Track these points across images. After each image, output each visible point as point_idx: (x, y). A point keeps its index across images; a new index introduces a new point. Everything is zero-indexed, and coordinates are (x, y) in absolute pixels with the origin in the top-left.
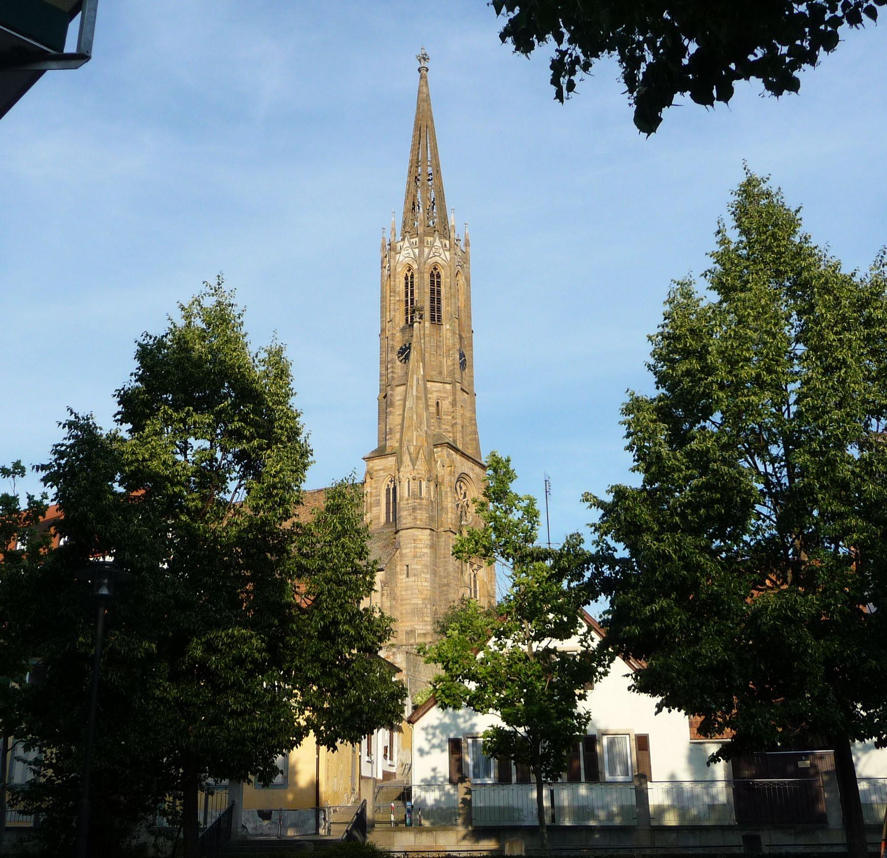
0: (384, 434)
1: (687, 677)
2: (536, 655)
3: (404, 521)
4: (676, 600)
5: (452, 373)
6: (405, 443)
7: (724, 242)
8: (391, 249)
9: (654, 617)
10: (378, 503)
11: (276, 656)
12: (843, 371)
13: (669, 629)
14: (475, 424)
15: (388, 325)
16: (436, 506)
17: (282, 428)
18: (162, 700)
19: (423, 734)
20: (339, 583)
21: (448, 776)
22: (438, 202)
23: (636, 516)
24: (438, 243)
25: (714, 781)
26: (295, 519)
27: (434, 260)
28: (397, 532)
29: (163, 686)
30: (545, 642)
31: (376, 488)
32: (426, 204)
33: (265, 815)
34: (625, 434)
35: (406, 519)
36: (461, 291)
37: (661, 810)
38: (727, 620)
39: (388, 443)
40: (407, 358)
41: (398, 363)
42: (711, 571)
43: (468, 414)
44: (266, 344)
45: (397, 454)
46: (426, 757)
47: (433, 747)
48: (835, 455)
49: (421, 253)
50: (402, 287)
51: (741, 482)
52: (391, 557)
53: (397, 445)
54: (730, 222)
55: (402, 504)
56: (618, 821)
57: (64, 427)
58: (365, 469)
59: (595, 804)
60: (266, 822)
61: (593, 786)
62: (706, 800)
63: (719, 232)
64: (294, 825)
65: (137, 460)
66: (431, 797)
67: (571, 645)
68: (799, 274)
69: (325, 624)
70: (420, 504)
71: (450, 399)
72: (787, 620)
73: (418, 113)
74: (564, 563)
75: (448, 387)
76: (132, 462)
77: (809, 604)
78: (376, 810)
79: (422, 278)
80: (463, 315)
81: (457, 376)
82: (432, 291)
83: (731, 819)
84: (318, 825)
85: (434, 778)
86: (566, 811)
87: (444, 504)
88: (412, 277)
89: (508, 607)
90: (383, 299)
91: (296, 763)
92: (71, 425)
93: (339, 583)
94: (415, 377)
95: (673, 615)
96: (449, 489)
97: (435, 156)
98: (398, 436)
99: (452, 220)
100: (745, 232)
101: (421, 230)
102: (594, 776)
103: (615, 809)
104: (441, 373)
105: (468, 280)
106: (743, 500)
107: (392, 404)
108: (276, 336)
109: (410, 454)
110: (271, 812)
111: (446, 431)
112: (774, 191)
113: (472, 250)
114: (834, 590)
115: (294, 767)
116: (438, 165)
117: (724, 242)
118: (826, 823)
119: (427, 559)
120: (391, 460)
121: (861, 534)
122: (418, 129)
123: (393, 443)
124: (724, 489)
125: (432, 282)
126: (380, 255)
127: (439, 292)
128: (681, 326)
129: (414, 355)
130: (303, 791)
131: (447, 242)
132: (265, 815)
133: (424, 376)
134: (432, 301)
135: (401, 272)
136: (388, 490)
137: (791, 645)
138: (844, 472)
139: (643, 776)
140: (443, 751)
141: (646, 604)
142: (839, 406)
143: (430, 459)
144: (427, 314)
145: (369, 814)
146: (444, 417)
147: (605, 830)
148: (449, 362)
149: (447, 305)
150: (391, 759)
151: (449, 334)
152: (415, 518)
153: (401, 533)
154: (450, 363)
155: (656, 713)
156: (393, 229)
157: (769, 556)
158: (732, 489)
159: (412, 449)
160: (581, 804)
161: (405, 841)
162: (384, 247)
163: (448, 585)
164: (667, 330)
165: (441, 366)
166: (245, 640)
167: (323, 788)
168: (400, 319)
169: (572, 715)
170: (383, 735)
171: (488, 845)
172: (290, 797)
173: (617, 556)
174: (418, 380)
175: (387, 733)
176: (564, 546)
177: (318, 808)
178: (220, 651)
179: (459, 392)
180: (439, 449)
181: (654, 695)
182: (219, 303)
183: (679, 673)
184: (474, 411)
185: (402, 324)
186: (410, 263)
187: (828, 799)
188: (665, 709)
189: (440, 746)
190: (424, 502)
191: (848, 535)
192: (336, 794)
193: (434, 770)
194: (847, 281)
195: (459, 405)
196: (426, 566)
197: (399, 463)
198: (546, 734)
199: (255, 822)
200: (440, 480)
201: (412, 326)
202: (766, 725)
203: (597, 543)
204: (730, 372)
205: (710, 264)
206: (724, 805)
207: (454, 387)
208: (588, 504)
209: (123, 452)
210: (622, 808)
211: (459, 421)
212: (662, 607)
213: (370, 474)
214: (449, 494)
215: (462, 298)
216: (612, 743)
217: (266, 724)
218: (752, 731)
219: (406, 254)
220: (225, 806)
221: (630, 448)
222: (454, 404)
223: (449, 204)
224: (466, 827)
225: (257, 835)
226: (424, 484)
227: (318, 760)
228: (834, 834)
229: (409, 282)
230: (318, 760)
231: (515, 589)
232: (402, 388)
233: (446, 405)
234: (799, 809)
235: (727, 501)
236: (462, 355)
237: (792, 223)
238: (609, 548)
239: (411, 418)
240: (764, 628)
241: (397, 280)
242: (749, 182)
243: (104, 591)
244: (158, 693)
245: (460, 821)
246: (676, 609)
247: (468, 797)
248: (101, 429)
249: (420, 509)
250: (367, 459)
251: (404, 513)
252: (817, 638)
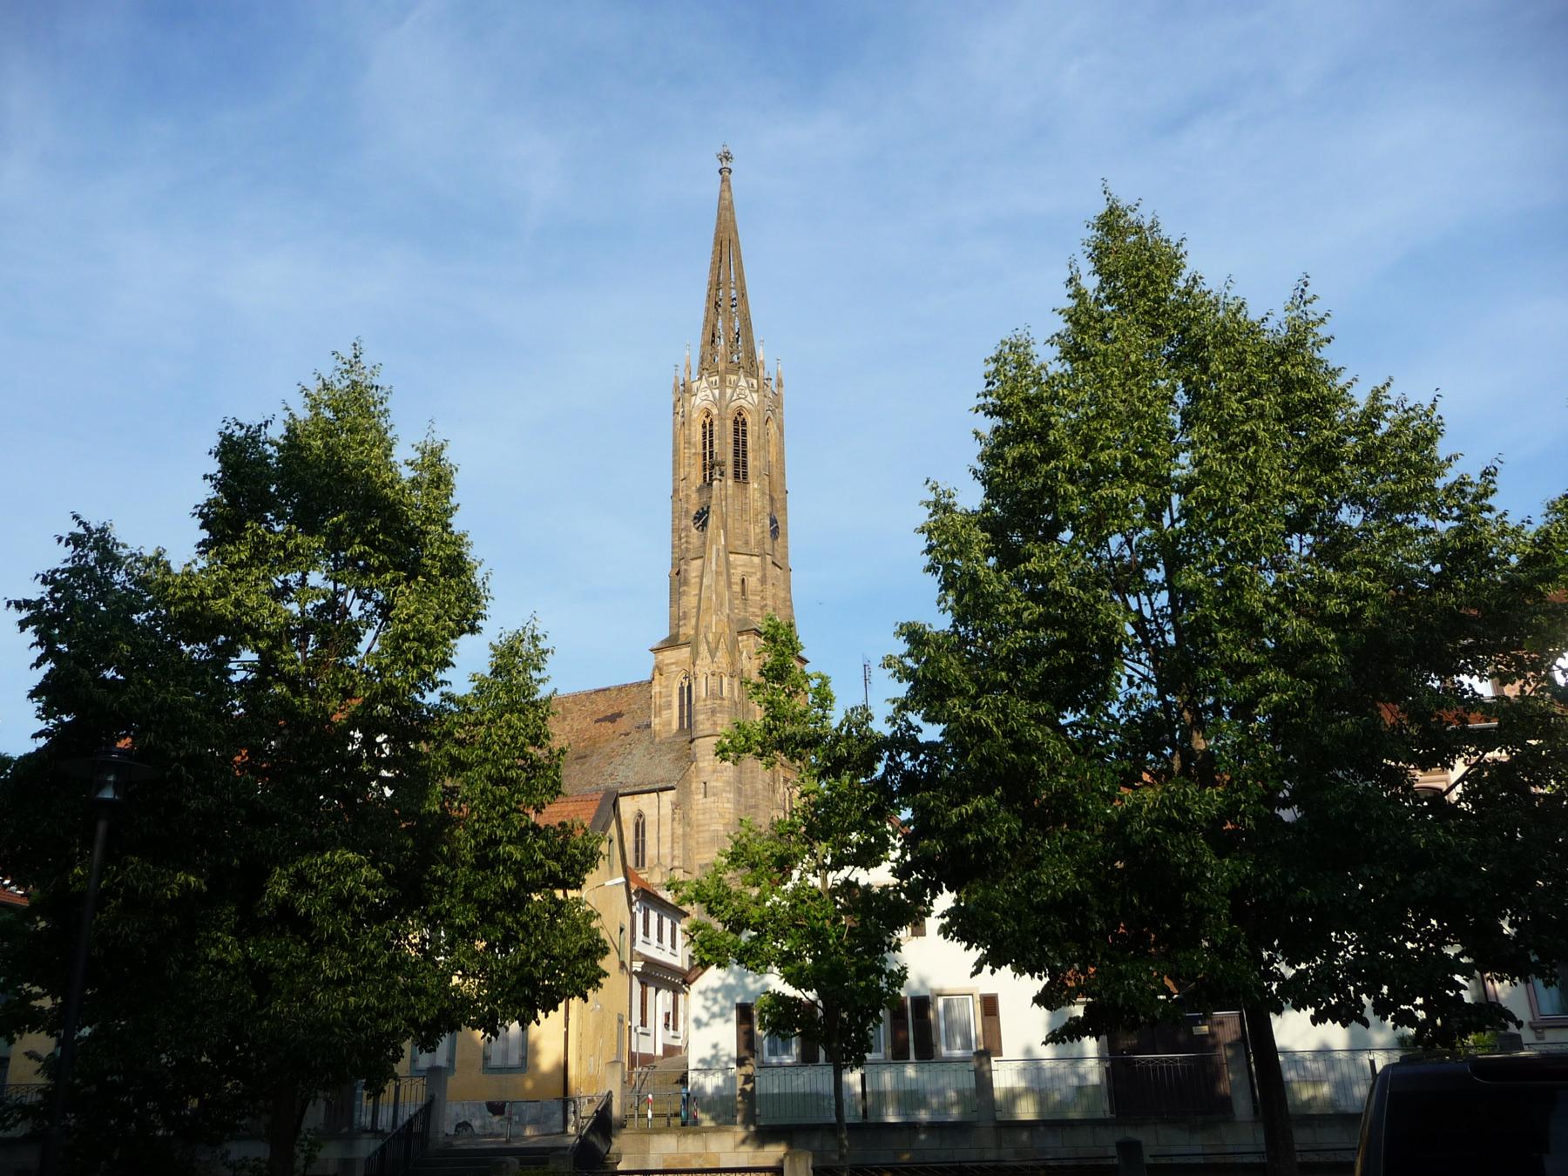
0: (677, 620)
1: (1018, 918)
2: (833, 892)
4: (1000, 800)
5: (761, 543)
6: (702, 630)
7: (1079, 295)
8: (685, 390)
9: (962, 827)
10: (669, 706)
11: (411, 892)
12: (1252, 450)
13: (989, 844)
15: (682, 484)
17: (434, 557)
18: (221, 964)
19: (701, 998)
20: (503, 781)
21: (734, 1054)
22: (743, 336)
23: (940, 670)
24: (743, 383)
25: (1082, 1058)
26: (445, 689)
27: (738, 403)
28: (692, 741)
29: (223, 943)
30: (846, 872)
32: (728, 338)
33: (496, 1108)
34: (925, 547)
36: (772, 442)
37: (1013, 1096)
38: (1082, 829)
39: (682, 631)
40: (705, 524)
42: (1055, 753)
43: (782, 594)
44: (419, 439)
45: (692, 643)
46: (703, 1030)
47: (713, 1016)
48: (1243, 572)
49: (722, 394)
50: (699, 437)
51: (1098, 612)
52: (685, 773)
53: (692, 632)
54: (1086, 266)
55: (698, 706)
56: (955, 1113)
57: (67, 544)
58: (653, 663)
59: (928, 1087)
60: (497, 1118)
61: (926, 1067)
62: (1074, 1081)
63: (1070, 281)
64: (535, 1122)
65: (191, 598)
66: (711, 1083)
67: (880, 876)
68: (1184, 331)
69: (478, 843)
71: (759, 575)
72: (1171, 826)
73: (719, 224)
74: (842, 750)
75: (756, 560)
76: (183, 600)
77: (1207, 800)
78: (623, 1106)
79: (723, 425)
80: (775, 472)
81: (768, 547)
82: (736, 442)
83: (1104, 1109)
84: (566, 1122)
85: (715, 1057)
86: (889, 1098)
88: (711, 424)
89: (790, 824)
90: (676, 452)
91: (538, 1038)
92: (75, 540)
93: (503, 781)
95: (998, 821)
97: (740, 276)
98: (693, 621)
99: (760, 354)
100: (1108, 276)
101: (721, 367)
102: (926, 1052)
103: (952, 1095)
104: (747, 543)
105: (780, 429)
106: (1102, 639)
107: (686, 582)
108: (434, 427)
110: (504, 1104)
111: (754, 614)
112: (1147, 224)
113: (784, 392)
114: (1245, 780)
115: (534, 1044)
116: (743, 288)
117: (1079, 295)
118: (1231, 1110)
120: (685, 652)
121: (1284, 692)
122: (719, 242)
123: (687, 630)
124: (1073, 625)
125: (736, 431)
126: (672, 399)
127: (745, 444)
128: (1011, 394)
129: (713, 520)
130: (546, 1077)
132: (496, 1108)
133: (726, 546)
134: (736, 453)
135: (698, 419)
136: (681, 689)
137: (1178, 866)
138: (1254, 600)
139: (990, 1049)
140: (727, 1021)
141: (953, 804)
142: (1247, 499)
143: (734, 649)
144: (730, 471)
145: (616, 1110)
147: (934, 1127)
148: (757, 530)
150: (675, 1028)
151: (757, 495)
152: (715, 724)
154: (758, 530)
155: (973, 975)
156: (688, 366)
157: (1149, 732)
158: (1084, 624)
160: (908, 1088)
161: (666, 1149)
162: (676, 388)
163: (756, 807)
164: (990, 400)
165: (747, 535)
166: (353, 868)
167: (572, 1072)
168: (696, 478)
169: (880, 972)
170: (664, 999)
171: (773, 1154)
172: (529, 1084)
173: (922, 738)
175: (670, 995)
176: (842, 725)
177: (565, 1098)
178: (315, 886)
179: (770, 566)
182: (355, 383)
183: (1004, 913)
184: (789, 590)
185: (699, 482)
187: (1233, 1081)
188: (987, 968)
189: (722, 1015)
191: (1264, 695)
192: (593, 1080)
193: (715, 1046)
194: (1253, 330)
195: (770, 582)
196: (729, 783)
197: (695, 654)
198: (844, 999)
199: (483, 1118)
201: (710, 484)
202: (1142, 991)
203: (891, 720)
204: (1084, 456)
205: (1060, 325)
206: (1095, 1086)
207: (763, 559)
208: (891, 671)
209: (168, 585)
210: (959, 1092)
211: (769, 602)
212: (976, 810)
213: (659, 669)
215: (773, 450)
216: (947, 1006)
217: (372, 1000)
218: (1120, 1001)
219: (704, 396)
220: (421, 1102)
221: (931, 569)
222: (763, 581)
223: (757, 337)
224: (747, 1128)
225: (485, 1136)
226: (725, 680)
227: (566, 1034)
228: (1243, 1137)
229: (708, 431)
230: (566, 1034)
231: (805, 799)
232: (699, 562)
233: (753, 582)
234: (1192, 1095)
235: (1076, 643)
236: (773, 521)
237: (1173, 264)
238: (910, 727)
240: (1136, 839)
242: (1111, 211)
243: (108, 794)
244: (214, 952)
245: (739, 1119)
246: (1002, 814)
247: (748, 1087)
248: (125, 546)
250: (656, 650)
251: (701, 717)
252: (1220, 855)
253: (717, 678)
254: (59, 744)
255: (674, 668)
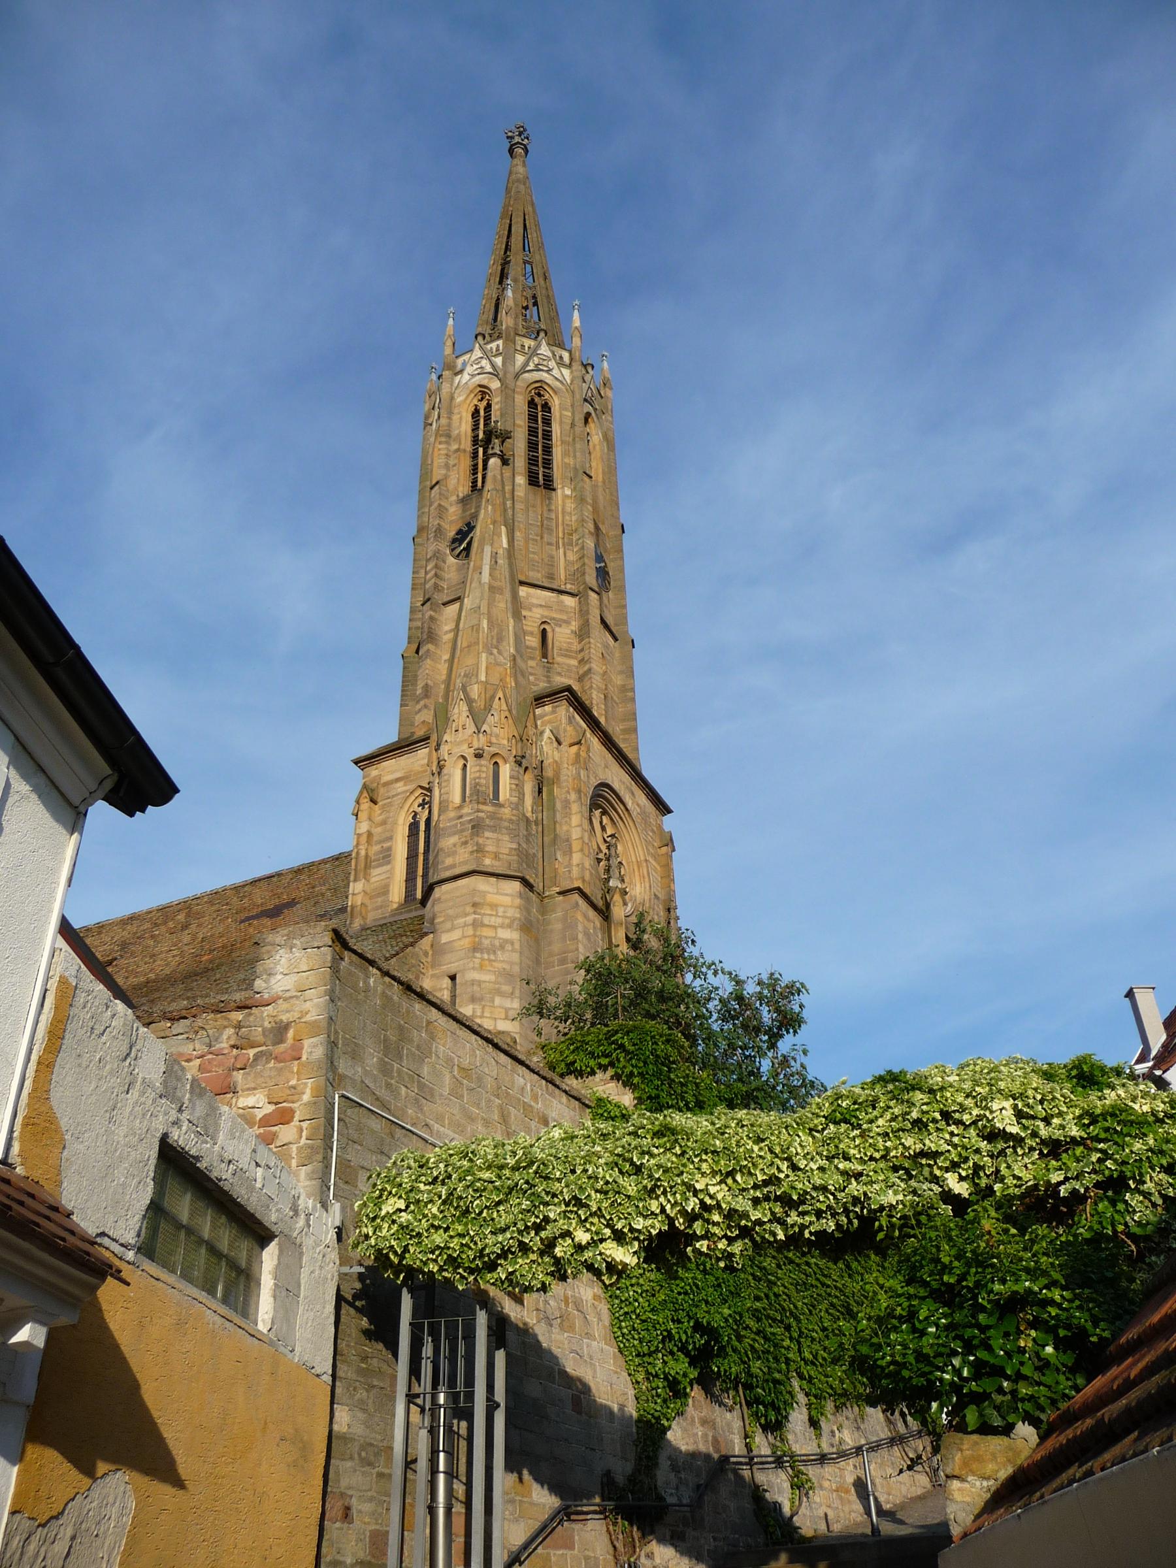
3: (449, 861)
10: (386, 856)
14: (633, 700)
16: (538, 833)
27: (537, 376)
31: (384, 823)
35: (454, 852)
41: (451, 560)
43: (618, 680)
70: (492, 816)
71: (574, 626)
75: (569, 601)
87: (562, 830)
88: (488, 407)
94: (488, 550)
96: (573, 796)
109: (469, 701)
119: (511, 959)
125: (533, 418)
127: (547, 435)
131: (566, 356)
146: (559, 659)
149: (565, 454)
151: (570, 505)
152: (480, 850)
153: (438, 892)
154: (572, 557)
159: (475, 691)
174: (494, 556)
180: (548, 708)
181: (776, 1558)
184: (630, 673)
185: (464, 489)
186: (485, 382)
190: (506, 812)
200: (549, 773)
214: (575, 807)
226: (506, 770)
233: (562, 636)
239: (476, 628)
241: (455, 417)
249: (494, 829)
253: (486, 764)
254: (804, 1540)
255: (400, 787)
